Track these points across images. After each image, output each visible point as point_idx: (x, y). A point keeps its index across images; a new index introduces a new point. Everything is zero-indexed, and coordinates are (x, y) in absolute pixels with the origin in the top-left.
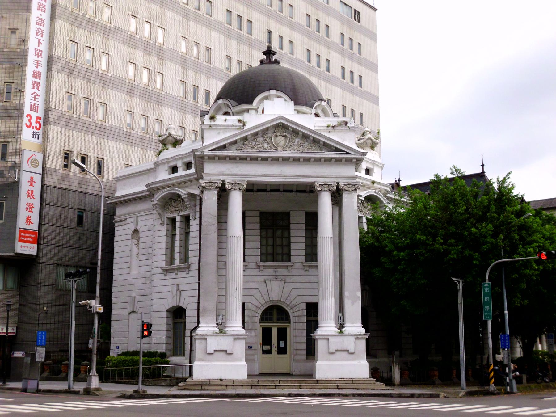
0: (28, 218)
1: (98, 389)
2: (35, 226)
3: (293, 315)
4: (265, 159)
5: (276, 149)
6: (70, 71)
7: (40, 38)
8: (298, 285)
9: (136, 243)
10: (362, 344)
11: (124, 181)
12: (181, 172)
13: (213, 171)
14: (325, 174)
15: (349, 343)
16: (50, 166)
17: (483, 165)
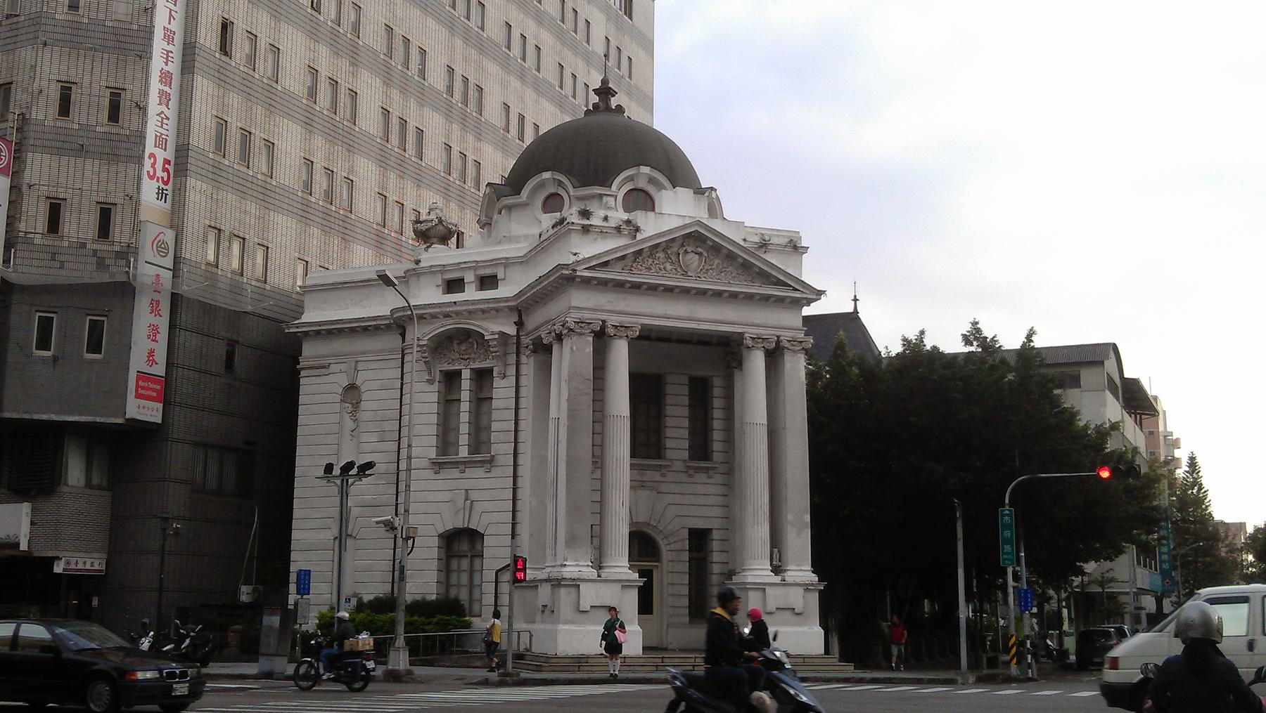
0: (151, 353)
1: (409, 672)
2: (160, 370)
3: (668, 548)
4: (669, 290)
5: (685, 274)
6: (222, 77)
7: (173, 7)
8: (678, 499)
9: (350, 409)
10: (814, 599)
11: (324, 295)
12: (471, 293)
13: (583, 304)
14: (757, 321)
15: (796, 598)
16: (188, 256)
17: (855, 300)
